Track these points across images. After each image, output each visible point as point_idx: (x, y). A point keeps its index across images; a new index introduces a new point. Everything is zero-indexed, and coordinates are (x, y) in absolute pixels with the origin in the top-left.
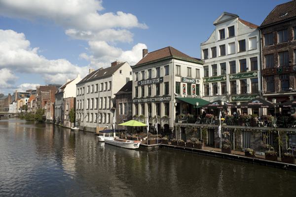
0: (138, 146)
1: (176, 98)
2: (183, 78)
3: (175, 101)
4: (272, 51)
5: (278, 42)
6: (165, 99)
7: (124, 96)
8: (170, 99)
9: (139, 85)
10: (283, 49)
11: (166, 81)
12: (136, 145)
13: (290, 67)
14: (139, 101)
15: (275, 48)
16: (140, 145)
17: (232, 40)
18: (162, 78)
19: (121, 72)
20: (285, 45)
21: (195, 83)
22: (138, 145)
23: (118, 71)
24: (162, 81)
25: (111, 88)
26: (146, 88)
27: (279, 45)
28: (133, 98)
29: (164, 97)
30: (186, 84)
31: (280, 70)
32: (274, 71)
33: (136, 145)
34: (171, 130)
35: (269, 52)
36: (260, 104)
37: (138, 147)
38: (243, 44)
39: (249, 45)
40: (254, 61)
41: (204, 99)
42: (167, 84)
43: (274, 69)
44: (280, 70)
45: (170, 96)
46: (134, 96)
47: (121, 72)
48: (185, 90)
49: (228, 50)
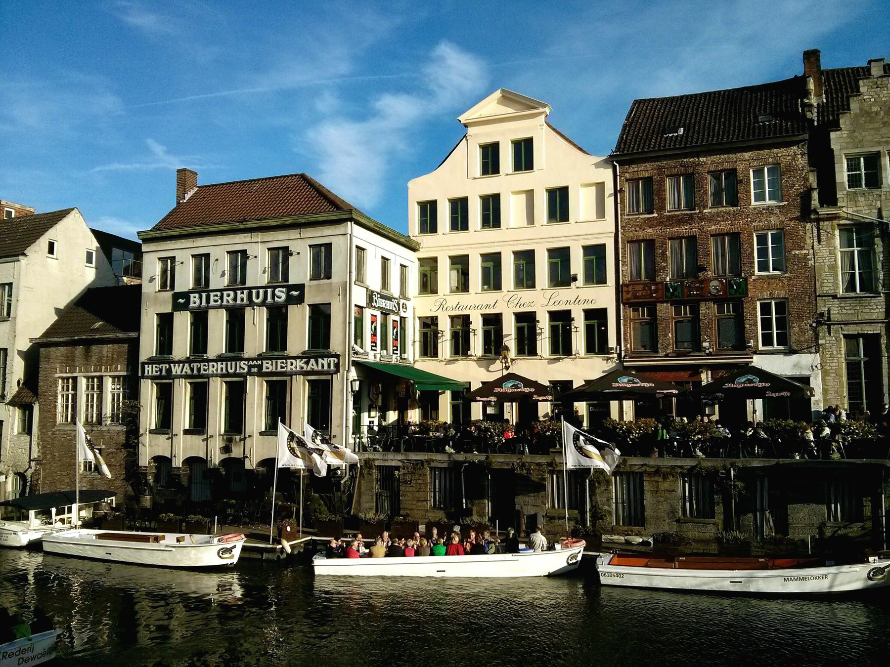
0: (234, 558)
1: (356, 364)
2: (372, 292)
3: (353, 374)
4: (650, 231)
5: (668, 208)
6: (312, 365)
7: (87, 355)
8: (337, 365)
9: (180, 301)
10: (683, 230)
11: (318, 300)
12: (229, 550)
13: (702, 282)
14: (176, 370)
15: (660, 223)
16: (244, 549)
17: (525, 180)
18: (301, 287)
19: (51, 250)
20: (689, 220)
21: (398, 314)
22: (237, 553)
23: (42, 243)
24: (300, 300)
25: (9, 314)
26: (218, 323)
27: (670, 218)
28: (143, 357)
29: (305, 356)
30: (378, 313)
31: (675, 289)
32: (656, 291)
33: (229, 550)
34: (145, 475)
35: (641, 234)
36: (761, 385)
37: (235, 560)
38: (559, 203)
39: (582, 203)
40: (595, 253)
41: (419, 366)
42: (320, 318)
43: (657, 284)
44: (675, 289)
45: (337, 356)
46: (148, 346)
47: (51, 250)
48: (374, 335)
49: (512, 210)
